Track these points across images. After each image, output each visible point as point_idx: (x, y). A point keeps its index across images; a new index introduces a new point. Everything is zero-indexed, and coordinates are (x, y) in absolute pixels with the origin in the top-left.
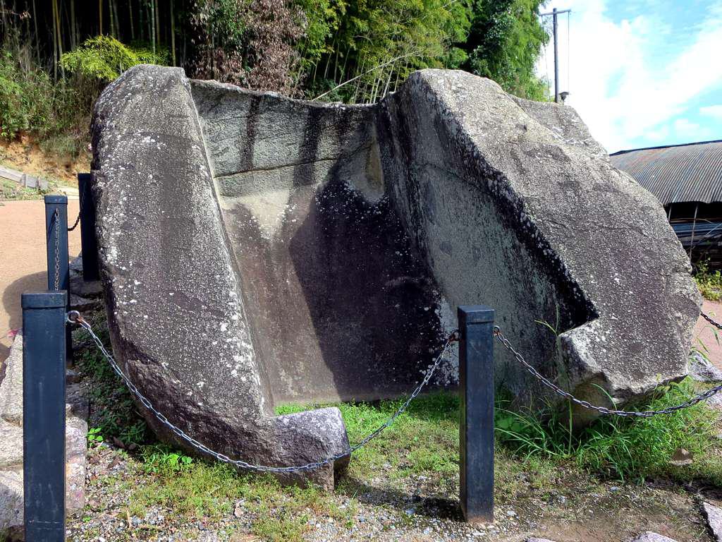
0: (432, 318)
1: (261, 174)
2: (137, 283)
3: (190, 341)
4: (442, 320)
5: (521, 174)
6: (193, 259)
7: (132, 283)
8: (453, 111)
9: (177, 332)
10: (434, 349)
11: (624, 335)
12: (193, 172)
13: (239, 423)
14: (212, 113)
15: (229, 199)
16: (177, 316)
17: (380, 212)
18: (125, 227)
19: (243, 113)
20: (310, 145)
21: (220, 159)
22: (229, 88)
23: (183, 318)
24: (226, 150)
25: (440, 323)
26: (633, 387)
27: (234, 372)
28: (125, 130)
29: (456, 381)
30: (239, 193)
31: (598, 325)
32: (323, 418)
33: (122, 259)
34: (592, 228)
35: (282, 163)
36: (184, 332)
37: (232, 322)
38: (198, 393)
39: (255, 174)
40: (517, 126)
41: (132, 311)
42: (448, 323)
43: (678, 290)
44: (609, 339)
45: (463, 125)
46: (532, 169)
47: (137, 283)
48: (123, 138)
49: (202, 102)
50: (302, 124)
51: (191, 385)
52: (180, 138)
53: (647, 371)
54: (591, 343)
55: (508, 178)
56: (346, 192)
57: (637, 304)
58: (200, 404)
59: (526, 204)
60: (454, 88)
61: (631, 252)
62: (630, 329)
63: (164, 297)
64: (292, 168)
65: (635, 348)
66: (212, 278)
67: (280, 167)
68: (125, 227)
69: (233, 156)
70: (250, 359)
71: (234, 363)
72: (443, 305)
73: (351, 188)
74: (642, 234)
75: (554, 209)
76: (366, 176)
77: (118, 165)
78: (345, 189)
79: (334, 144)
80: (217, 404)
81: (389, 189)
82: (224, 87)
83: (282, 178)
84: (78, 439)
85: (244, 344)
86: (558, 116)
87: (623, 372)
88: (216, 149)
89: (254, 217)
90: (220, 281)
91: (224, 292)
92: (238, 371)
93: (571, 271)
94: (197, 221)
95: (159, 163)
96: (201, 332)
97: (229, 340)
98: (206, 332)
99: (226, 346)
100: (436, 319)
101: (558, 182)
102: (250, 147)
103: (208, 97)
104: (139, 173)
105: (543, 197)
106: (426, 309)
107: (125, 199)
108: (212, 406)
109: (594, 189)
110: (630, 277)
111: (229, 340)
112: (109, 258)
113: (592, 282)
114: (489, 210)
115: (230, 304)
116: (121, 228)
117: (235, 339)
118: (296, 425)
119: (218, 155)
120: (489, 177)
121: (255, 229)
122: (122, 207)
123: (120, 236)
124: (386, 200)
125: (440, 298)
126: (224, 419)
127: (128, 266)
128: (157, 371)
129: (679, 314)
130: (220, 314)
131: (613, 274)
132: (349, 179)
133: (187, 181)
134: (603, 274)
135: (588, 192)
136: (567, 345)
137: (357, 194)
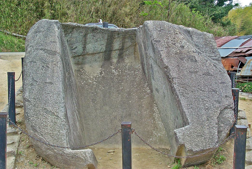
6: (52, 97)
19: (82, 34)
21: (74, 51)
24: (76, 48)
39: (87, 56)
88: (72, 47)
119: (73, 49)
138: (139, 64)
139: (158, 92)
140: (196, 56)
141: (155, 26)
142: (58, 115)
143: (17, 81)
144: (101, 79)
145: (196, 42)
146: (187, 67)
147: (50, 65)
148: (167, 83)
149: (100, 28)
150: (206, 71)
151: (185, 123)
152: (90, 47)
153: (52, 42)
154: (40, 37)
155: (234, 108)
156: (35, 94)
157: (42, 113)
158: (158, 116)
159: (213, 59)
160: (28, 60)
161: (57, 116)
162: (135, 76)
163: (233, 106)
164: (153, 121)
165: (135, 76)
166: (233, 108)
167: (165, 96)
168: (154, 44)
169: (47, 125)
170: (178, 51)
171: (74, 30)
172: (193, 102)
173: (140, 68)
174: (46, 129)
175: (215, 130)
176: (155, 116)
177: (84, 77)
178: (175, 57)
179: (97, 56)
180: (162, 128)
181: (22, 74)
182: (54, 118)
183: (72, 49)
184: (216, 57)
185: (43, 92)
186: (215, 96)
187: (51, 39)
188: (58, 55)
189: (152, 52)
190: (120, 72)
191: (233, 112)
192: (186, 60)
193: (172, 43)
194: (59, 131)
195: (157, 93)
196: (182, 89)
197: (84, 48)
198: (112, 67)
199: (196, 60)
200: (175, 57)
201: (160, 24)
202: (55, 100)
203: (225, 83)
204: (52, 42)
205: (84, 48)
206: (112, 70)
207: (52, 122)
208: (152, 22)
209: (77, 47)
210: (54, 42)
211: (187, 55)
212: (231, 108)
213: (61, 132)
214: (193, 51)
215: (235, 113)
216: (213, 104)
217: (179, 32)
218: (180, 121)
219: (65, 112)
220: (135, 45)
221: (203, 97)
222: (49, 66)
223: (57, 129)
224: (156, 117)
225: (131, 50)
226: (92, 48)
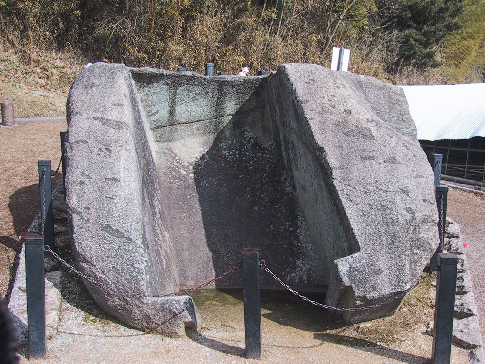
8: (301, 99)
20: (219, 106)
21: (153, 118)
22: (157, 72)
24: (157, 112)
29: (304, 281)
35: (198, 119)
39: (178, 127)
40: (345, 110)
43: (421, 235)
55: (326, 152)
60: (306, 80)
69: (164, 113)
74: (408, 195)
79: (236, 104)
82: (154, 71)
84: (55, 302)
88: (151, 112)
112: (71, 203)
119: (152, 115)
120: (317, 149)
128: (94, 270)
129: (418, 251)
136: (336, 267)
138: (271, 140)
139: (305, 191)
140: (372, 129)
141: (299, 74)
142: (131, 237)
144: (203, 167)
145: (372, 102)
146: (356, 149)
147: (112, 147)
148: (321, 177)
150: (389, 156)
153: (114, 105)
154: (93, 96)
156: (87, 199)
157: (102, 234)
158: (304, 234)
159: (403, 134)
160: (73, 138)
161: (130, 239)
162: (263, 163)
163: (436, 218)
164: (296, 243)
165: (263, 163)
166: (435, 222)
167: (317, 199)
168: (297, 106)
169: (112, 255)
170: (341, 120)
172: (366, 212)
173: (273, 147)
174: (109, 262)
175: (405, 261)
176: (300, 235)
177: (174, 165)
178: (336, 130)
179: (195, 125)
180: (313, 255)
181: (61, 165)
182: (123, 243)
183: (150, 115)
184: (407, 130)
185: (103, 197)
186: (405, 200)
187: (114, 99)
188: (127, 129)
189: (295, 121)
190: (237, 154)
191: (436, 228)
192: (354, 136)
193: (330, 105)
194: (132, 265)
195: (304, 194)
196: (348, 188)
197: (172, 113)
198: (222, 146)
199: (371, 135)
200: (336, 130)
201: (308, 71)
202: (124, 209)
203: (424, 177)
204: (114, 105)
205: (172, 113)
206: (223, 151)
207: (121, 249)
208: (293, 66)
209: (158, 110)
210: (118, 105)
211: (357, 127)
213: (136, 266)
214: (368, 120)
215: (440, 230)
217: (343, 85)
218: (345, 246)
219: (142, 231)
220: (264, 106)
221: (384, 202)
222: (111, 148)
223: (129, 261)
224: (301, 235)
226: (187, 113)
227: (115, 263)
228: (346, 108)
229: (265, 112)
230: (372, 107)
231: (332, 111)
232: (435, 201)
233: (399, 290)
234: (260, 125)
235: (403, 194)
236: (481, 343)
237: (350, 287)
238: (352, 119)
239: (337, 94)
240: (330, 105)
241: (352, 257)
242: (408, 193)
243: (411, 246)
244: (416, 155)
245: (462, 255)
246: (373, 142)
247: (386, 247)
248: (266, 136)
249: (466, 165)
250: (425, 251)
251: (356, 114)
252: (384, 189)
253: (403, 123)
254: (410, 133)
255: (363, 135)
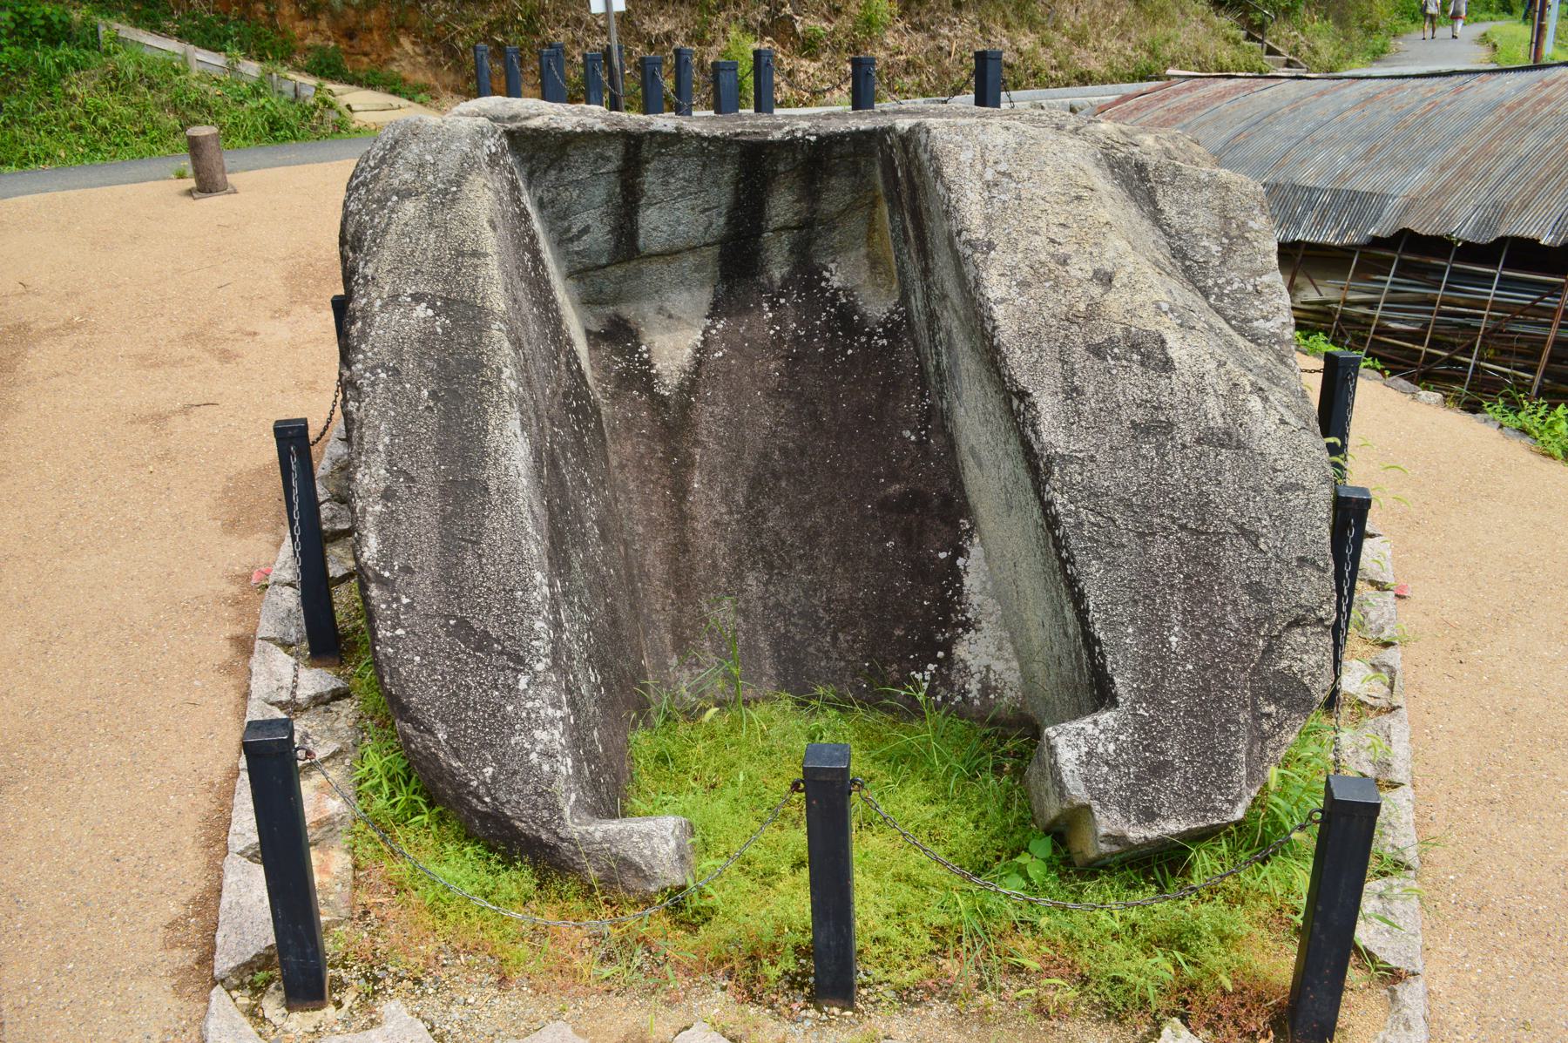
0: (949, 575)
1: (655, 266)
2: (405, 601)
3: (475, 703)
4: (967, 581)
5: (1066, 399)
6: (484, 561)
7: (397, 600)
9: (458, 687)
10: (943, 634)
11: (1148, 745)
12: (490, 383)
13: (537, 831)
14: (553, 172)
15: (598, 310)
16: (459, 660)
17: (885, 342)
18: (388, 495)
19: (611, 167)
21: (576, 247)
23: (467, 663)
24: (586, 230)
25: (962, 584)
26: (1131, 834)
27: (533, 756)
28: (387, 288)
30: (617, 299)
31: (1111, 722)
32: (648, 836)
33: (385, 557)
34: (1165, 528)
36: (468, 687)
37: (536, 675)
38: (484, 783)
40: (1096, 273)
41: (398, 649)
42: (977, 587)
43: (1284, 663)
44: (1120, 750)
45: (984, 275)
46: (1090, 389)
47: (405, 601)
48: (384, 306)
49: (532, 158)
50: (728, 172)
51: (477, 771)
52: (473, 306)
53: (1164, 812)
54: (1087, 753)
56: (823, 290)
57: (1191, 690)
58: (487, 799)
59: (1057, 469)
60: (989, 175)
61: (1221, 584)
62: (1165, 734)
63: (441, 627)
64: (716, 250)
65: (1159, 770)
66: (510, 597)
67: (692, 249)
68: (388, 495)
70: (557, 736)
71: (534, 742)
72: (973, 551)
73: (836, 282)
74: (1257, 546)
75: (1106, 484)
76: (868, 256)
77: (375, 367)
78: (823, 284)
80: (508, 802)
81: (904, 298)
83: (697, 269)
85: (550, 711)
86: (1224, 209)
87: (1124, 809)
88: (568, 229)
89: (644, 348)
90: (522, 601)
91: (526, 623)
92: (540, 754)
93: (1097, 616)
94: (492, 485)
95: (439, 365)
96: (491, 688)
97: (529, 705)
98: (497, 689)
99: (524, 714)
100: (957, 575)
101: (1133, 422)
102: (631, 220)
103: (542, 148)
104: (408, 386)
105: (1092, 456)
106: (942, 555)
107: (387, 440)
108: (502, 804)
109: (1198, 441)
110: (1198, 635)
111: (529, 705)
113: (1128, 641)
114: (1014, 445)
115: (534, 643)
116: (382, 497)
117: (538, 703)
118: (611, 843)
119: (571, 240)
121: (646, 374)
122: (383, 455)
123: (381, 512)
124: (900, 314)
125: (971, 536)
126: (517, 823)
127: (391, 571)
129: (1272, 709)
130: (520, 660)
131: (1170, 629)
132: (833, 262)
133: (481, 402)
134: (1153, 627)
135: (1184, 446)
137: (846, 297)
143: (318, 439)
149: (698, 135)
151: (1100, 694)
152: (656, 225)
155: (1334, 619)
163: (1328, 612)
166: (1327, 623)
171: (569, 150)
172: (1139, 593)
179: (690, 260)
183: (562, 240)
184: (1269, 325)
186: (1247, 560)
192: (1116, 358)
196: (1093, 520)
212: (1321, 620)
216: (1235, 603)
225: (856, 224)
227: (484, 726)
228: (1097, 266)
229: (876, 217)
230: (1172, 249)
231: (1057, 277)
232: (1331, 562)
233: (1216, 821)
234: (863, 251)
235: (1243, 541)
236: (1419, 968)
237: (1088, 807)
238: (1115, 302)
239: (1075, 221)
240: (1053, 256)
241: (1095, 723)
242: (1258, 538)
243: (1255, 694)
244: (1286, 418)
245: (1391, 649)
246: (1170, 378)
247: (1190, 697)
248: (879, 285)
249: (1420, 351)
250: (1293, 706)
251: (1125, 285)
252: (1191, 525)
253: (1256, 303)
254: (1274, 334)
255: (1142, 355)
